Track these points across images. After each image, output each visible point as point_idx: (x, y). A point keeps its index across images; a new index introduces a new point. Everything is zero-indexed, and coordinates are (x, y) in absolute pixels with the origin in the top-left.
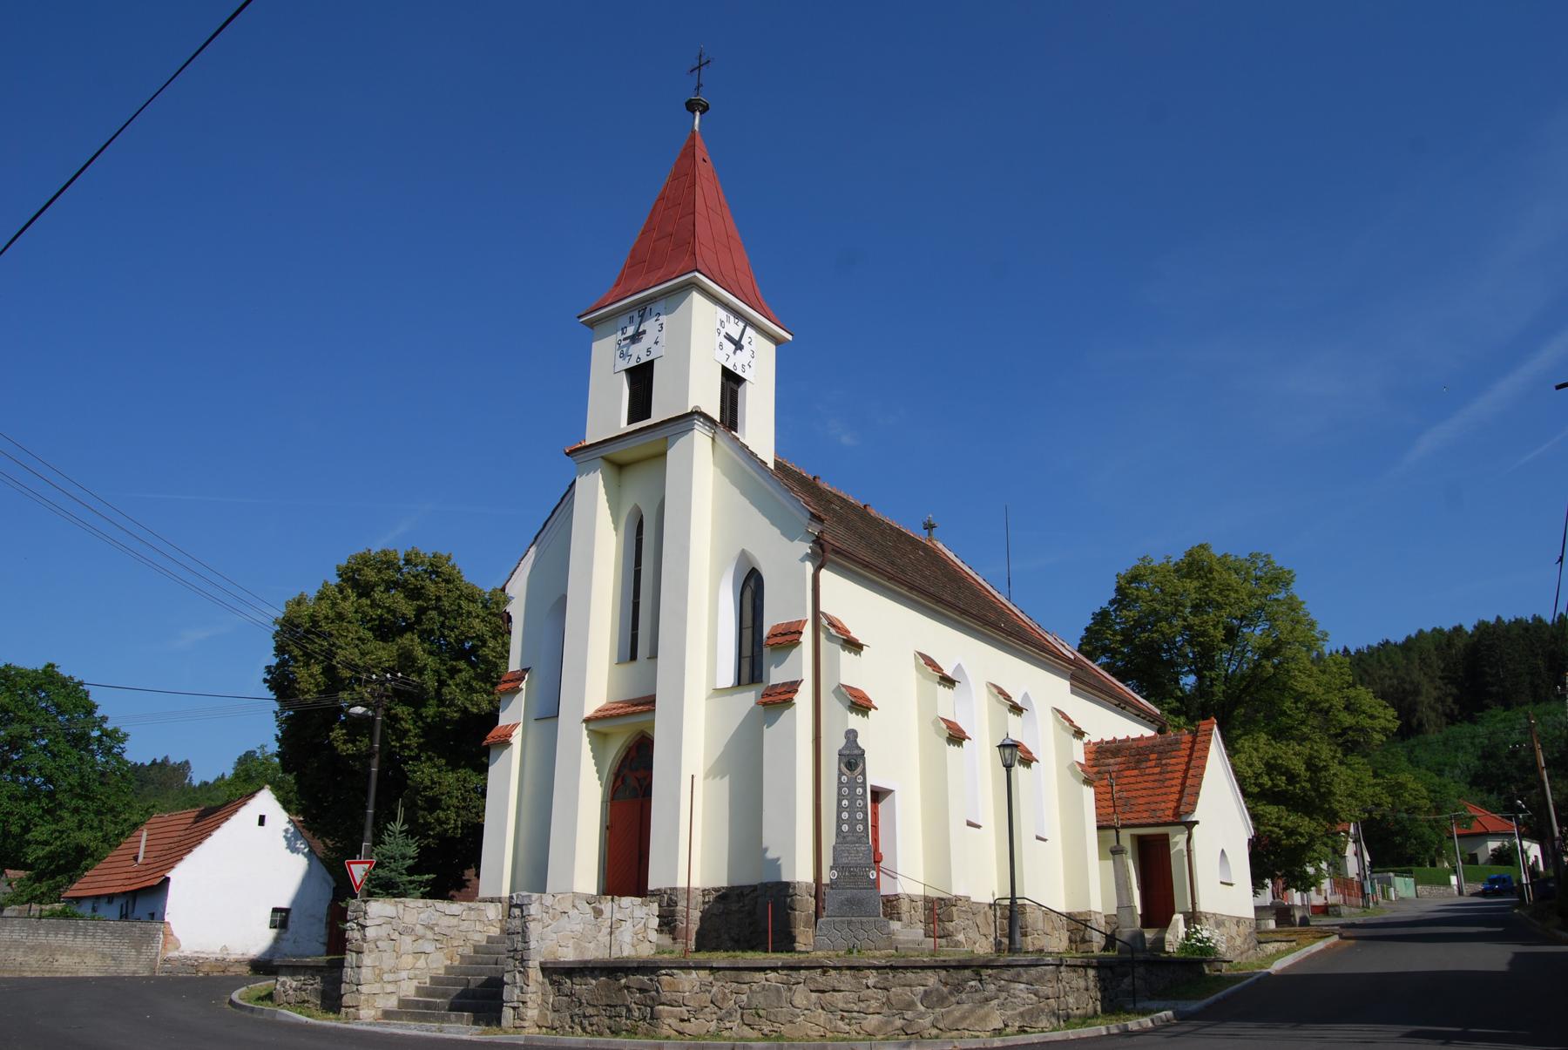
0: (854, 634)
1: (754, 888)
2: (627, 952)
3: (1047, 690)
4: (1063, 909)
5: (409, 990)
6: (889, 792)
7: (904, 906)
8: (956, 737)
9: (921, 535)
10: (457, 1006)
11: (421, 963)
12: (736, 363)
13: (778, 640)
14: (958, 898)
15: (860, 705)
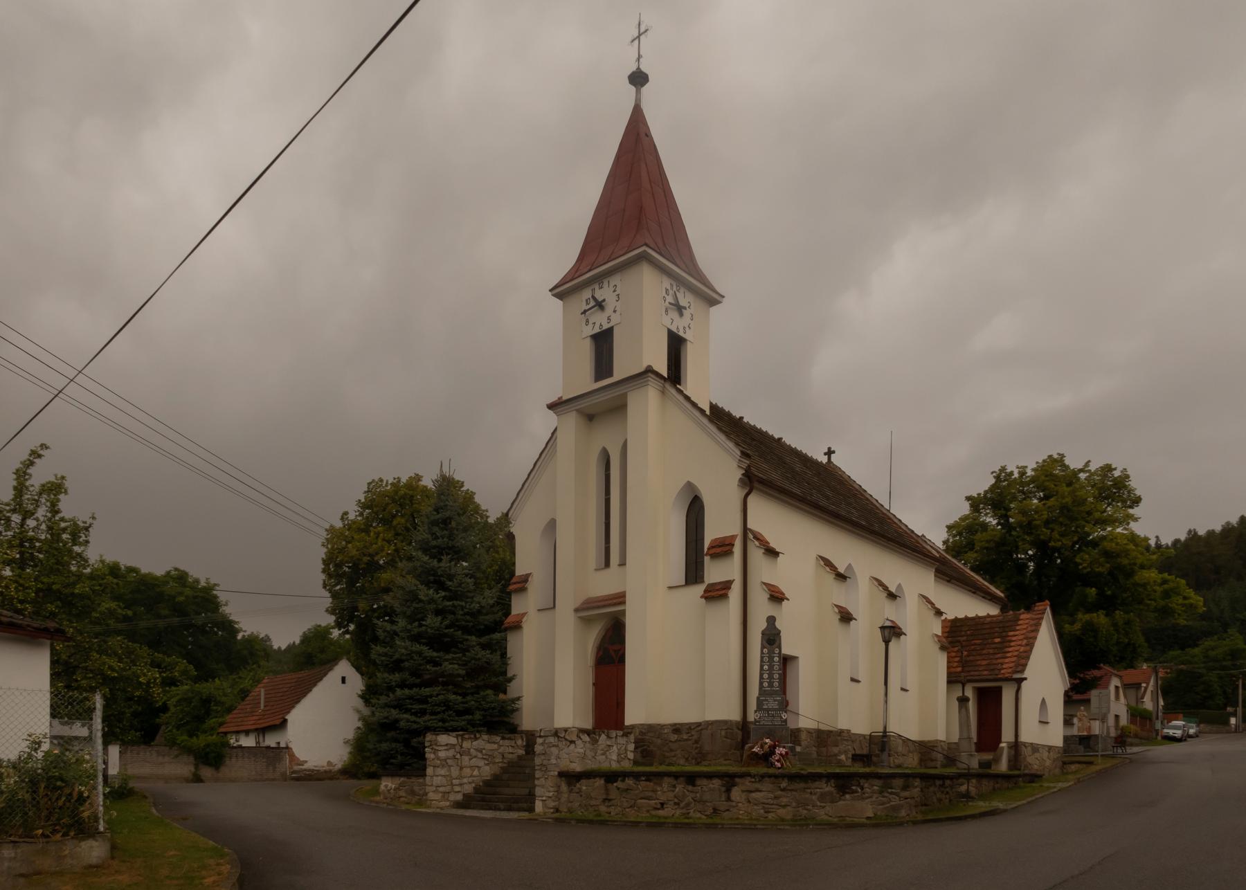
0: (773, 545)
1: (699, 724)
2: (615, 766)
3: (916, 581)
4: (914, 736)
5: (469, 789)
6: (795, 658)
7: (803, 736)
8: (846, 617)
9: (824, 459)
10: (1101, 678)
11: (476, 773)
12: (678, 325)
13: (718, 550)
14: (842, 731)
15: (777, 597)
